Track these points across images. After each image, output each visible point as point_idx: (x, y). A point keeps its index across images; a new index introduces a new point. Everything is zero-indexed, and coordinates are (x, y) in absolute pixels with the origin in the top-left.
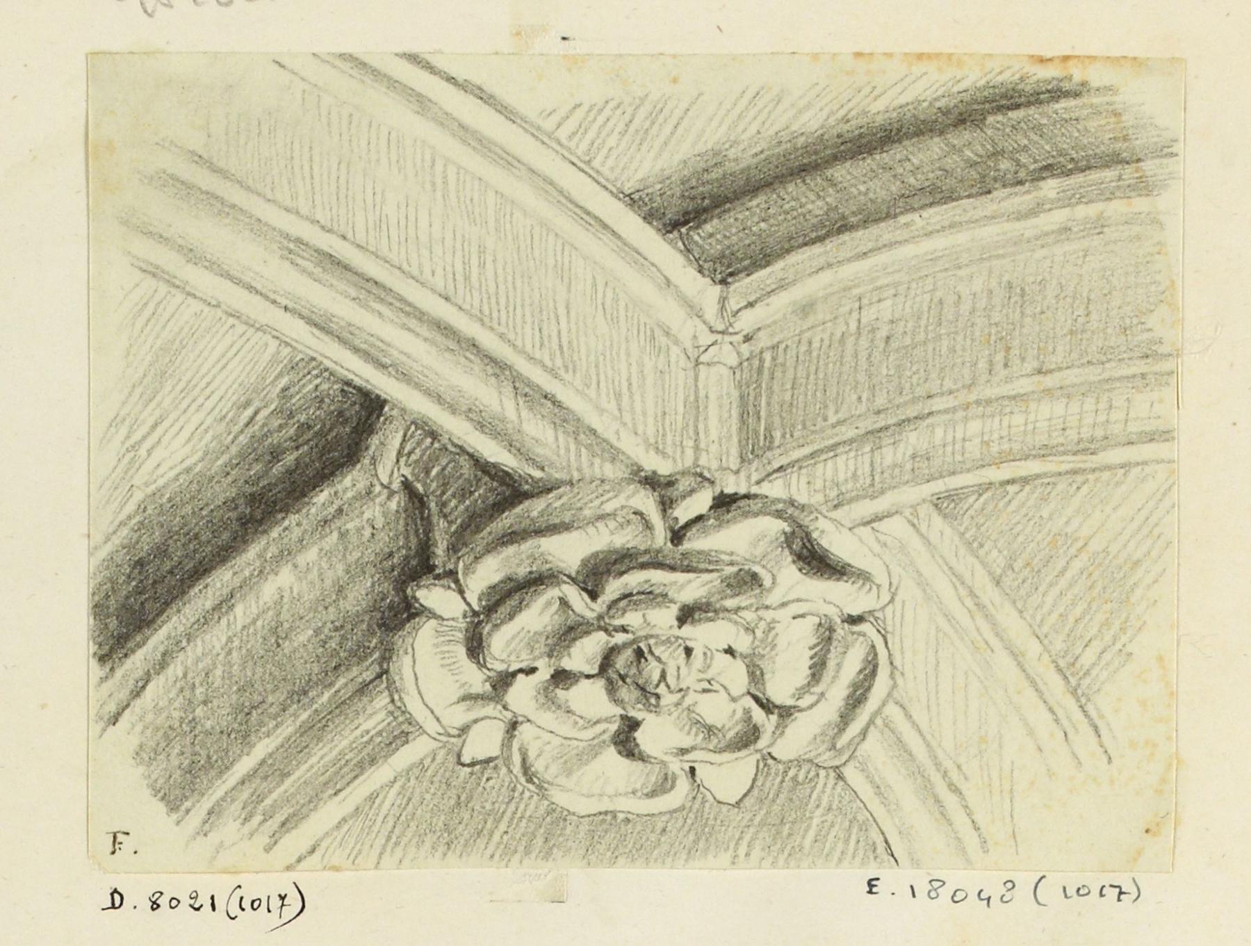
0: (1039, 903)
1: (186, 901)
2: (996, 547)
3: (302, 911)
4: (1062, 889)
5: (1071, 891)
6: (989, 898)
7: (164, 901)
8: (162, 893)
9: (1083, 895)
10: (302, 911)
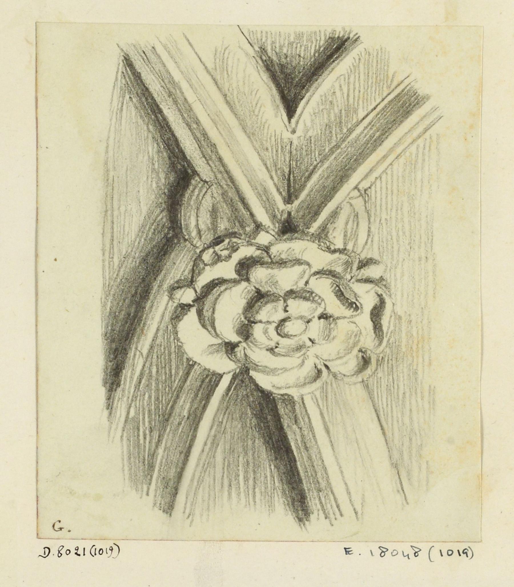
0: (431, 561)
1: (73, 551)
2: (210, 384)
3: (472, 557)
4: (439, 551)
5: (445, 553)
6: (408, 555)
7: (63, 552)
8: (63, 547)
9: (394, 555)
10: (472, 557)
